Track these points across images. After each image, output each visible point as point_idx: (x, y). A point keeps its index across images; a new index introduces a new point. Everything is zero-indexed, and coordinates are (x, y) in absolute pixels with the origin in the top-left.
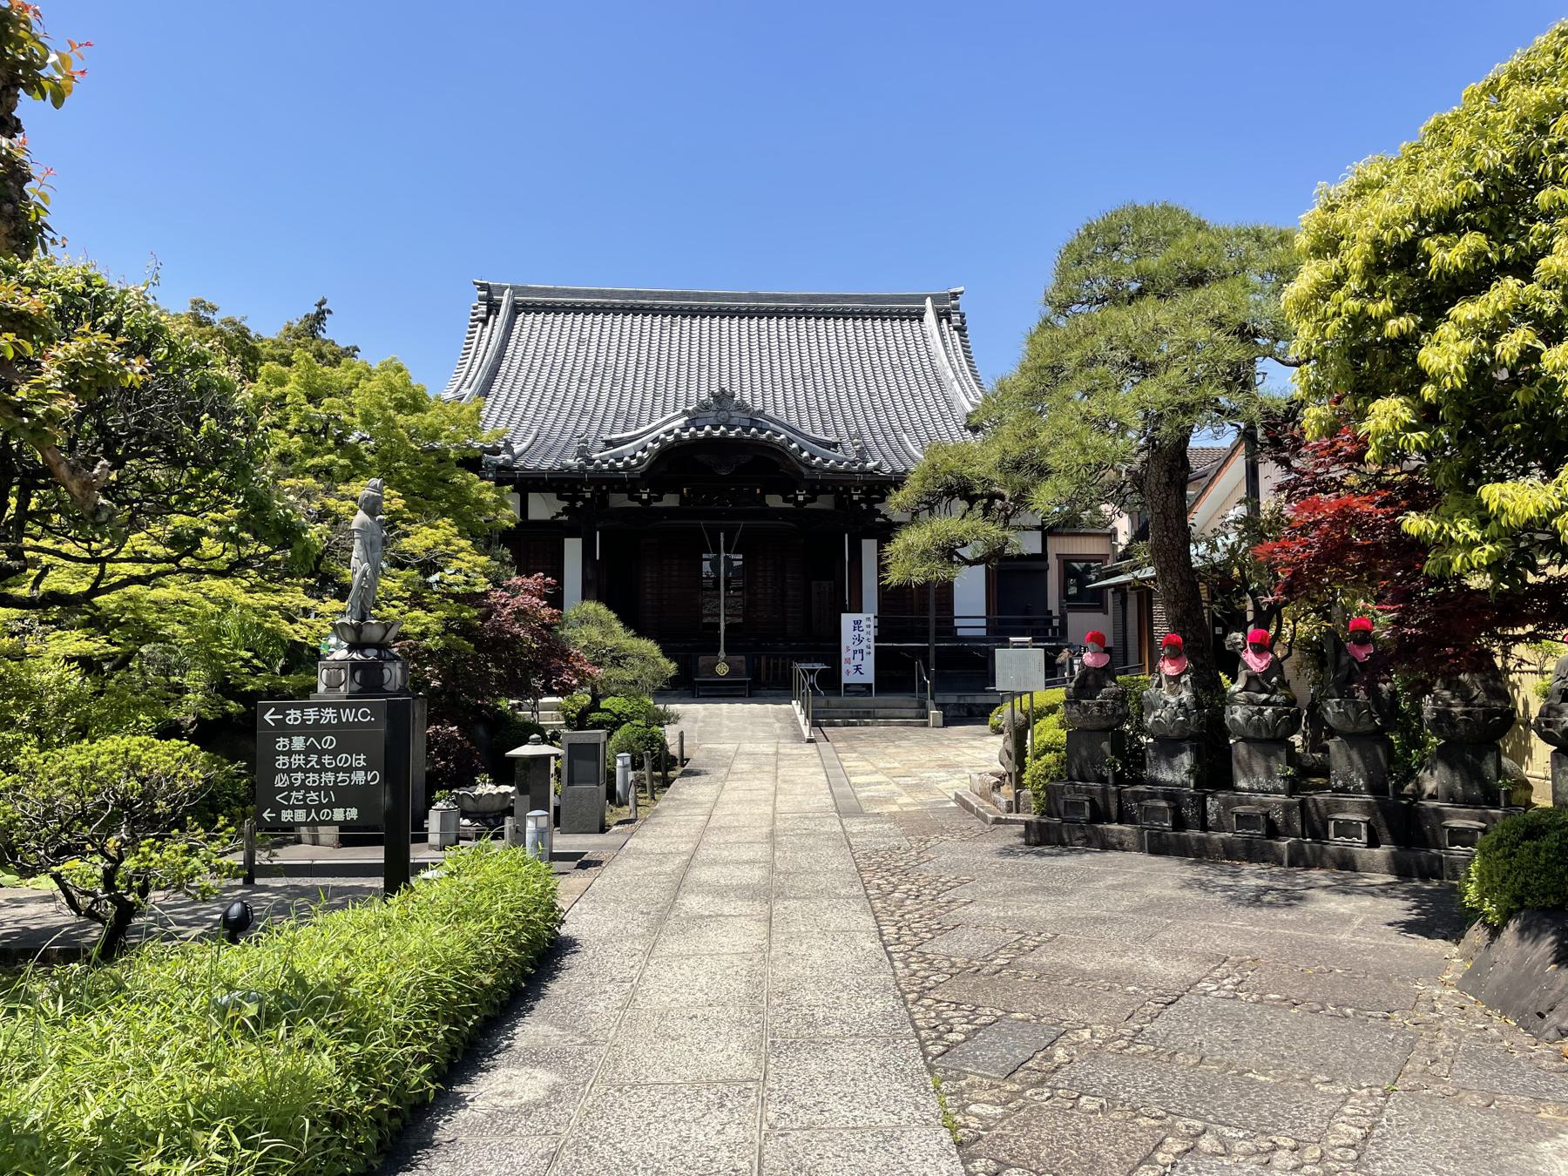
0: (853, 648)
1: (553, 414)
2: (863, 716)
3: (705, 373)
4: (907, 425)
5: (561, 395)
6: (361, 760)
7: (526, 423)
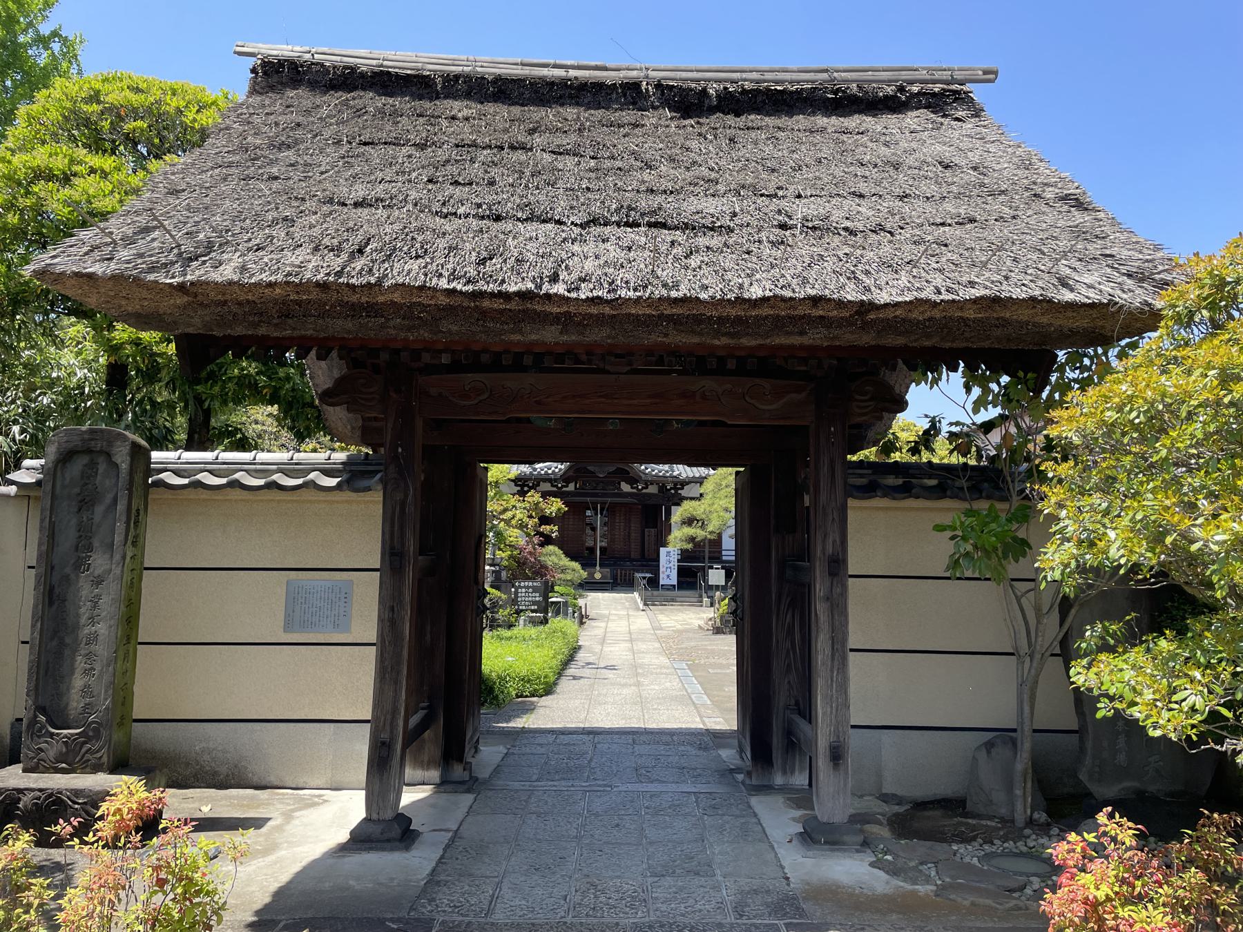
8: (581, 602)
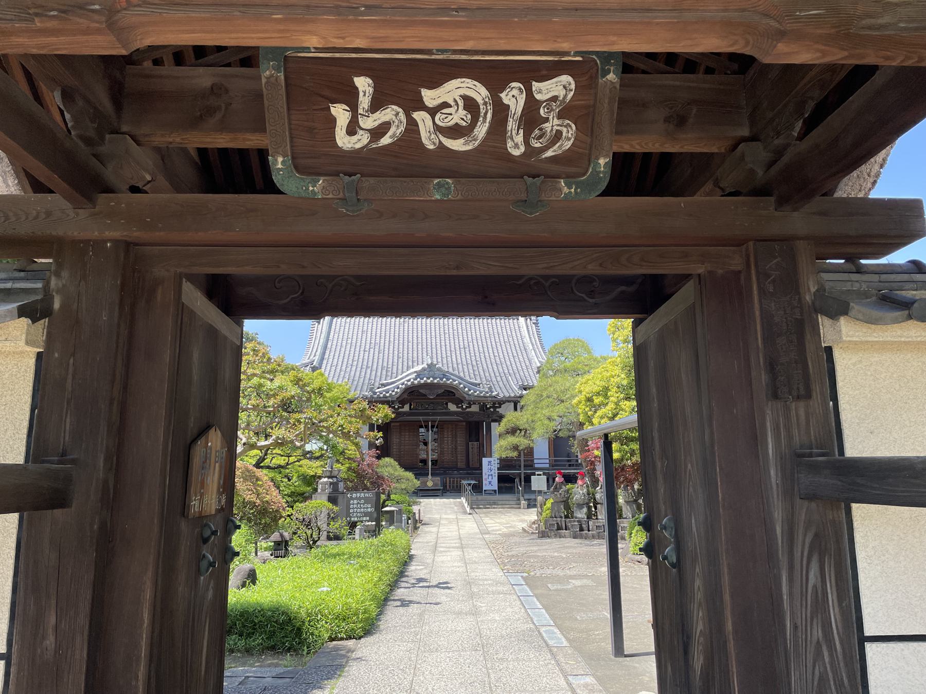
1: (354, 368)
2: (493, 504)
3: (420, 346)
4: (511, 372)
5: (356, 358)
6: (369, 506)
7: (342, 373)
8: (415, 509)
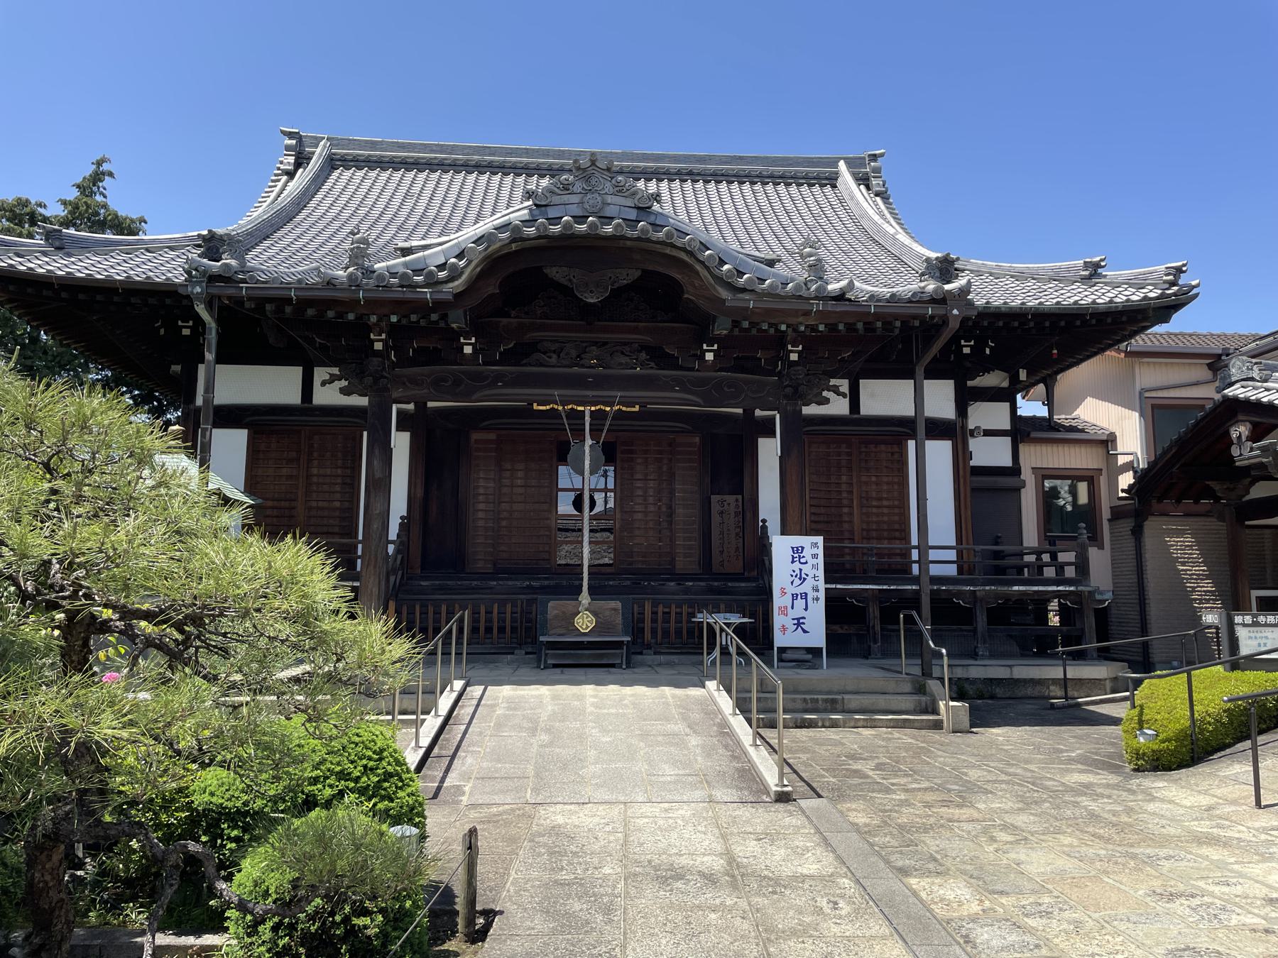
0: (791, 590)
